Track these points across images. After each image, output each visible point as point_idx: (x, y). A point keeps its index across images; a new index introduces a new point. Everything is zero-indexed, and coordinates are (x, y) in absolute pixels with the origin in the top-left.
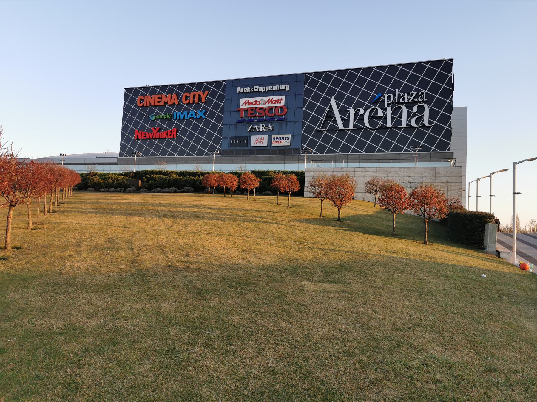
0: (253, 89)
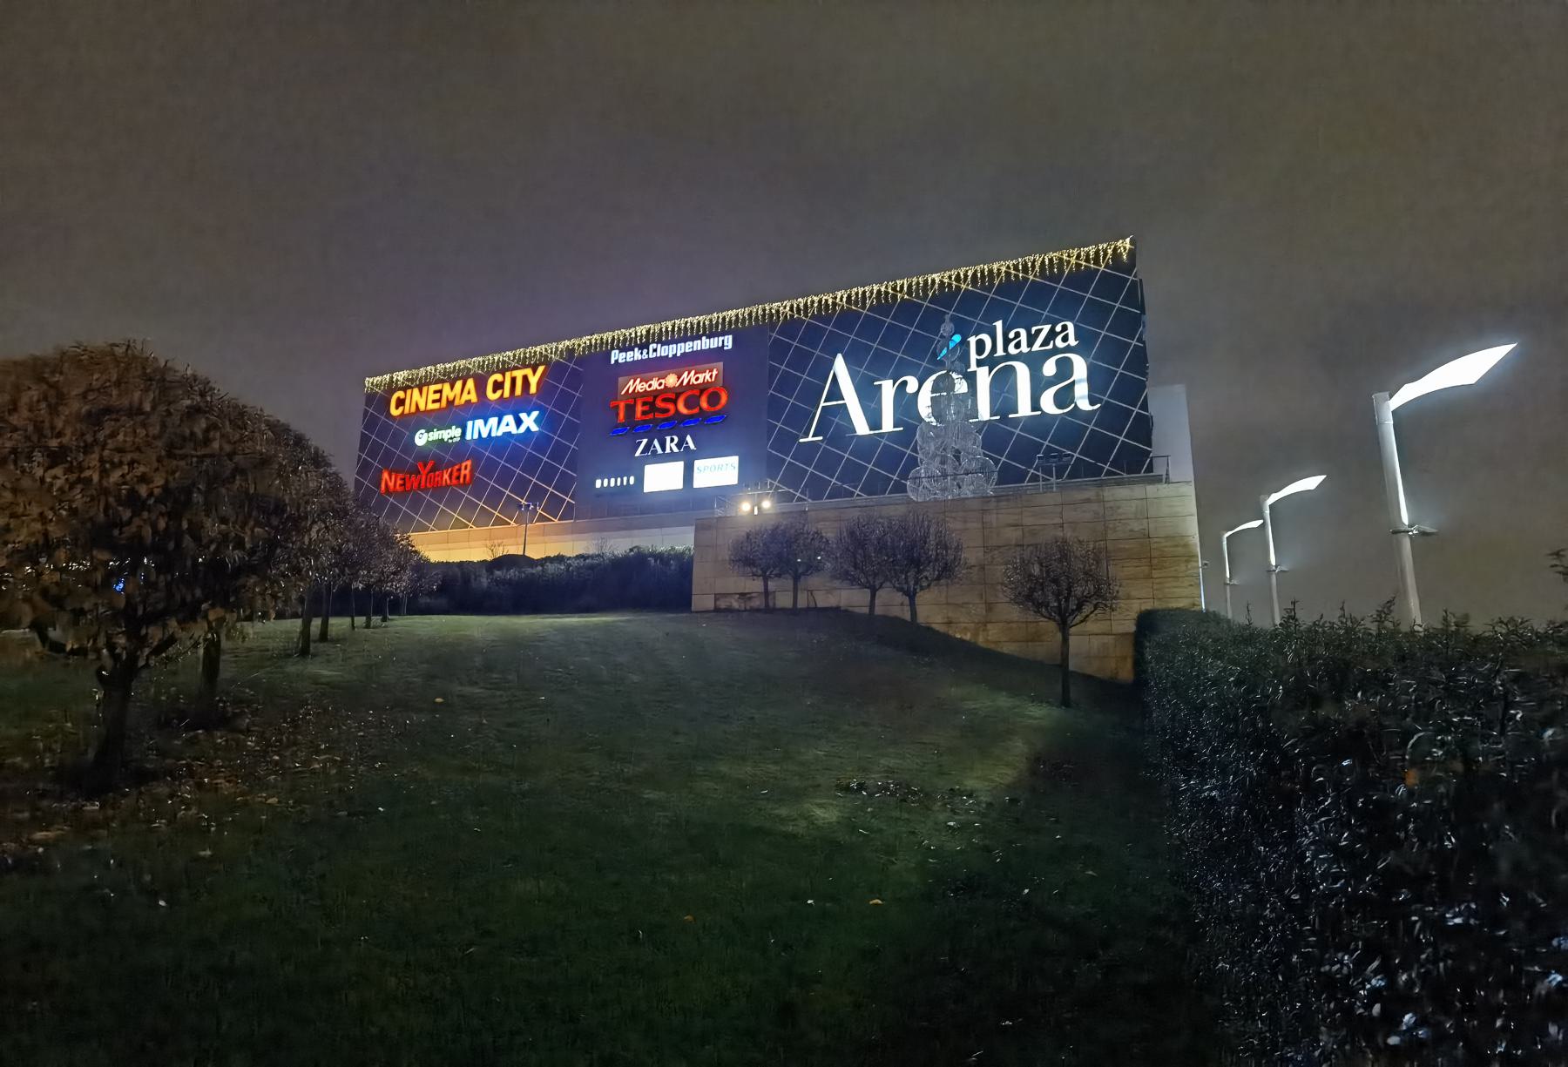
0: (648, 353)
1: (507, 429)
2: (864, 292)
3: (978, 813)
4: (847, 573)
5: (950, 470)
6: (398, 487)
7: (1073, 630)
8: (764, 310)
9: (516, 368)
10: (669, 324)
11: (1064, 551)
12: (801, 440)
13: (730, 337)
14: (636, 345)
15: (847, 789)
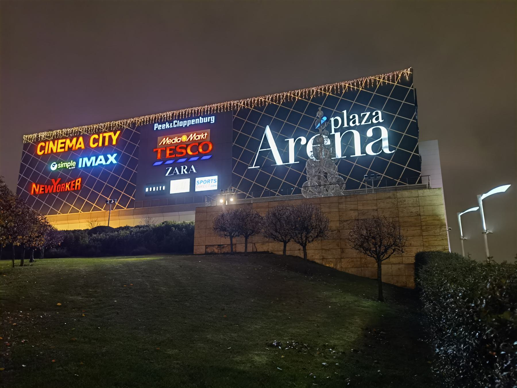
0: (173, 125)
1: (101, 162)
2: (279, 96)
3: (338, 358)
4: (272, 234)
5: (322, 183)
6: (41, 192)
7: (383, 262)
8: (230, 104)
9: (105, 132)
10: (184, 111)
11: (377, 221)
12: (249, 168)
13: (214, 117)
14: (167, 121)
15: (272, 345)
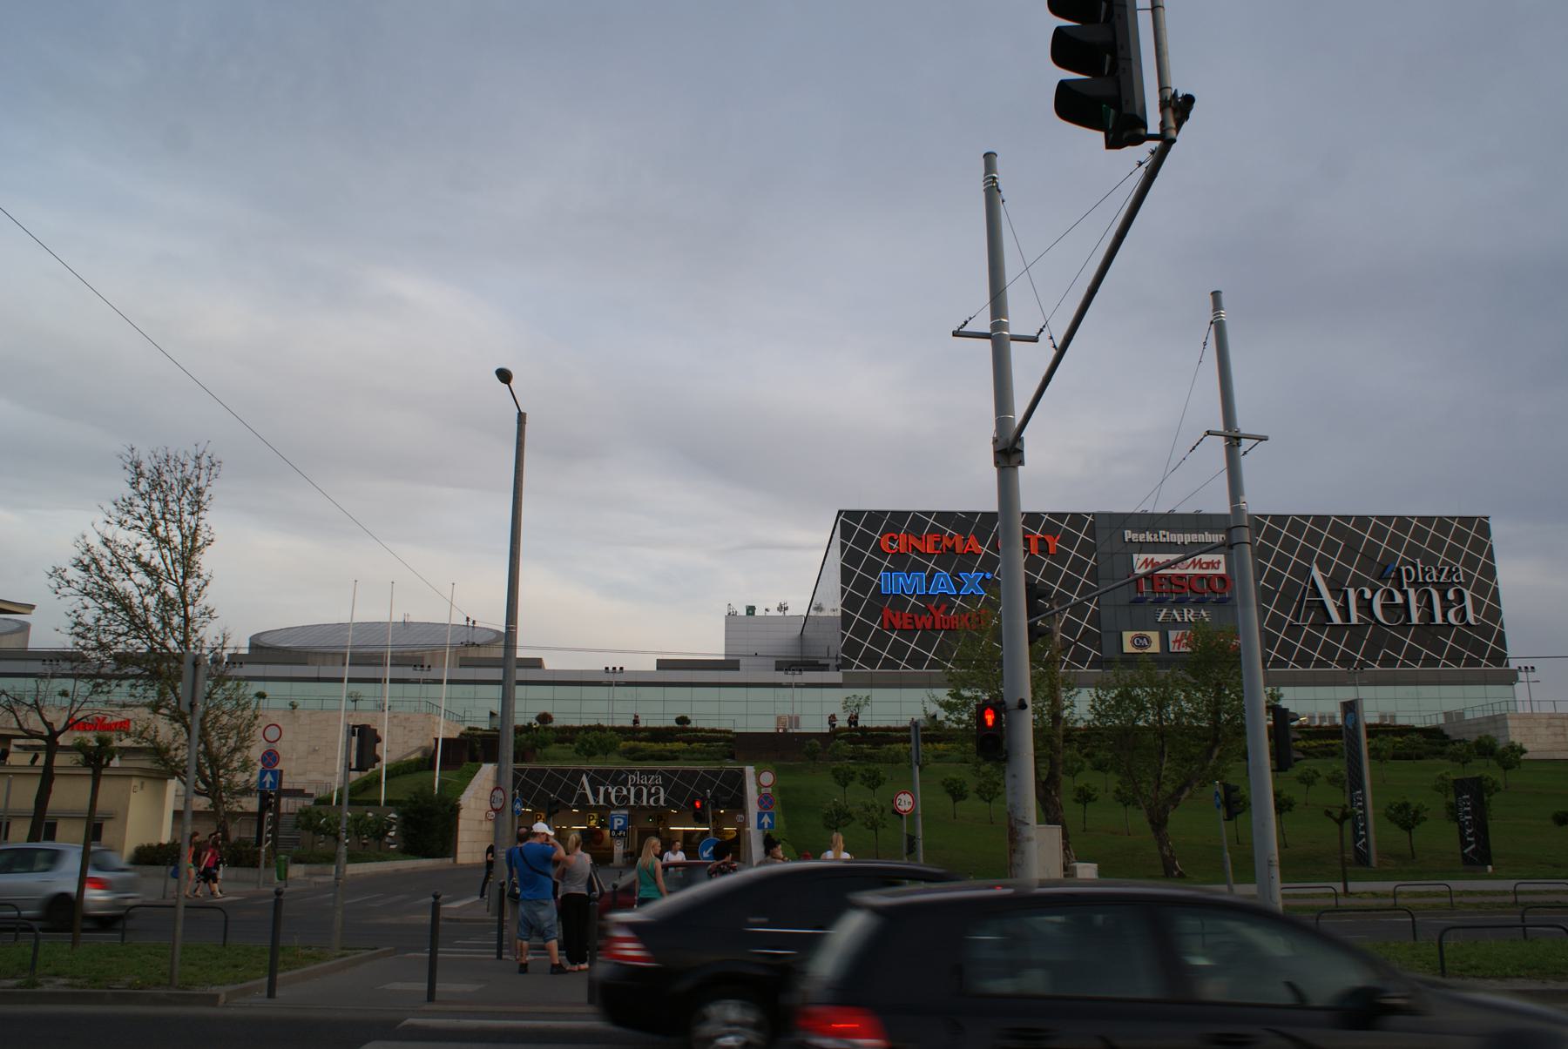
0: (1158, 537)
